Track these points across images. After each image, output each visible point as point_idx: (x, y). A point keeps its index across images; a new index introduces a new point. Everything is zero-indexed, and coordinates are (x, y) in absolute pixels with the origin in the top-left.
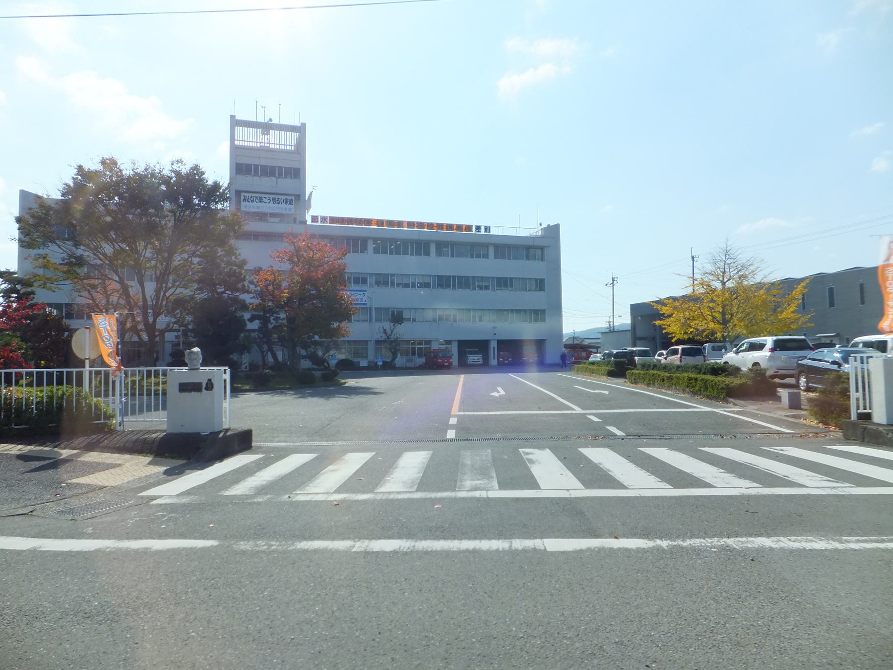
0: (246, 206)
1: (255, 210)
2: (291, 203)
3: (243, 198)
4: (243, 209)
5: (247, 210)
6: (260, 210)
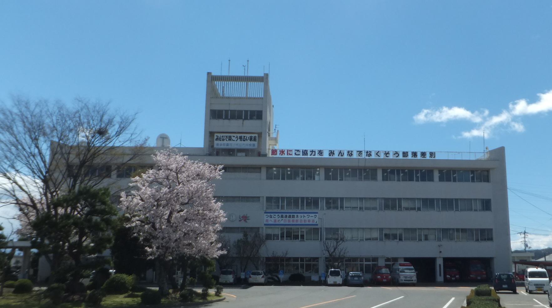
0: (217, 145)
1: (225, 147)
2: (255, 140)
3: (215, 137)
4: (215, 146)
5: (220, 147)
6: (229, 147)
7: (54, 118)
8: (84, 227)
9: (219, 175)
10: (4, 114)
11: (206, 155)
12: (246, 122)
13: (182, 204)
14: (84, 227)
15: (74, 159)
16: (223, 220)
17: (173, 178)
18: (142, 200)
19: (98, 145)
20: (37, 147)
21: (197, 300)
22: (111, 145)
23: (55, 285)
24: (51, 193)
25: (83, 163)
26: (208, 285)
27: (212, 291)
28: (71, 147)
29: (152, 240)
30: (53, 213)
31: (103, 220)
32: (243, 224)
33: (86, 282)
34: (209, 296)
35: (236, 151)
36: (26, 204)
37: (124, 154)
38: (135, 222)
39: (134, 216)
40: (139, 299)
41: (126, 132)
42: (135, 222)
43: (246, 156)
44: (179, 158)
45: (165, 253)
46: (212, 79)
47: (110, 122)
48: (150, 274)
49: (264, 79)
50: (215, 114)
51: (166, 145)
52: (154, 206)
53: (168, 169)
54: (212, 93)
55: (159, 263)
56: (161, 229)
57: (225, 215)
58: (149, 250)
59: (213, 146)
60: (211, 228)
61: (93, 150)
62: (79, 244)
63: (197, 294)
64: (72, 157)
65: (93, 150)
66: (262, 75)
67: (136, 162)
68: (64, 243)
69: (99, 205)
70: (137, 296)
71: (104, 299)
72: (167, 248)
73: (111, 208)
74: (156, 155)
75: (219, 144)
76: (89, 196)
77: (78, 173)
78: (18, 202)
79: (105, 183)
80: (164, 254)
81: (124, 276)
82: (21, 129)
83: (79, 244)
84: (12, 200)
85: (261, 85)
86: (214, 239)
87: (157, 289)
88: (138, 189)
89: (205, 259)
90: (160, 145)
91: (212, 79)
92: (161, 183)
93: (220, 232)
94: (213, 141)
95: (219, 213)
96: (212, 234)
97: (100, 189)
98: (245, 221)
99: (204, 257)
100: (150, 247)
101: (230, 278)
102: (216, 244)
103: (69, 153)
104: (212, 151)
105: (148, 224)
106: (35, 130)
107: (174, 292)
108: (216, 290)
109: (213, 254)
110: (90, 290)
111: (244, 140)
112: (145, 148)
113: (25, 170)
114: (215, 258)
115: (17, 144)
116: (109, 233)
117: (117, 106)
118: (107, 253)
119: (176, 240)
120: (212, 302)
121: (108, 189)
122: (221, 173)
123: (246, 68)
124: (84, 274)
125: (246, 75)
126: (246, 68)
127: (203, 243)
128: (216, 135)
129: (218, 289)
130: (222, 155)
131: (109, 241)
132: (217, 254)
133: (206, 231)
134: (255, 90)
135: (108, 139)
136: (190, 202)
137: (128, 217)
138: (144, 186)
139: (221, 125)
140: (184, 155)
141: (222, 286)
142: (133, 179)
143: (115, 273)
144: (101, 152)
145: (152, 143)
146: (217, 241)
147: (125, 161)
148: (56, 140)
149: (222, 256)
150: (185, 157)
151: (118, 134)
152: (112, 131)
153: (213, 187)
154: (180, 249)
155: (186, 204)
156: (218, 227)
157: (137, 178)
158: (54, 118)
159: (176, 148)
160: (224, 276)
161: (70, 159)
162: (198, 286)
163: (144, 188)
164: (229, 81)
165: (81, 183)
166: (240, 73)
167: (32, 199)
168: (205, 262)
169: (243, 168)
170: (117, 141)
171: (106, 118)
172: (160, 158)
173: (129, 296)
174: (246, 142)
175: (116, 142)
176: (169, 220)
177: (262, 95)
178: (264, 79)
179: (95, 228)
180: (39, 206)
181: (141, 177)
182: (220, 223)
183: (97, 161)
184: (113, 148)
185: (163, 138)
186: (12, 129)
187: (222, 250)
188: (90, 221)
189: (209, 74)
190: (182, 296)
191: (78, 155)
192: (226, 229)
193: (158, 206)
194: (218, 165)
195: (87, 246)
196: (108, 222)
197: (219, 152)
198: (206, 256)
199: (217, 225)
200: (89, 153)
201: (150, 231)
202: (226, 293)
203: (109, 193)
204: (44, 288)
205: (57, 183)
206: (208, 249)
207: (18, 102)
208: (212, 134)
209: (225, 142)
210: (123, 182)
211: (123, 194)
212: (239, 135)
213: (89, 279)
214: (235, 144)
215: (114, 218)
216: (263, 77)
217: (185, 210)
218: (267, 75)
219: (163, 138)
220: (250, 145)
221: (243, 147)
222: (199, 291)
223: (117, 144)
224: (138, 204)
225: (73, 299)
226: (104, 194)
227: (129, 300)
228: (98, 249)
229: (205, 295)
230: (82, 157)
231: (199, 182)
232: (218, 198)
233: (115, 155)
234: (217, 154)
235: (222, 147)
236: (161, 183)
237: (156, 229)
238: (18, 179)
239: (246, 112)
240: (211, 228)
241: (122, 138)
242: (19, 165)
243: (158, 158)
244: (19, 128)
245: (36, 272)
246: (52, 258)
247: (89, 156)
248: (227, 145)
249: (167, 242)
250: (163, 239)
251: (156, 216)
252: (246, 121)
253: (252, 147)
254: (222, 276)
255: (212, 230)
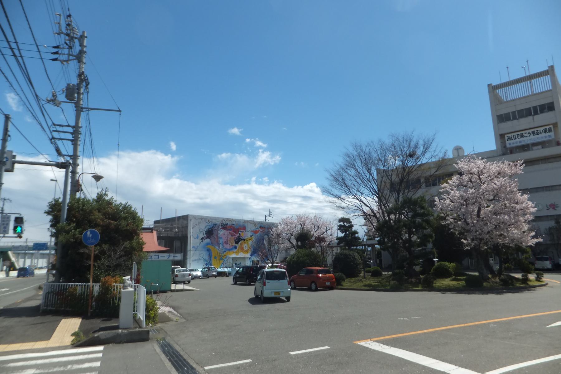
0: (510, 144)
1: (519, 144)
2: (550, 130)
3: (506, 138)
4: (508, 146)
5: (512, 146)
6: (523, 143)
7: (379, 152)
8: (411, 227)
9: (521, 170)
10: (349, 157)
11: (500, 155)
12: (536, 117)
13: (489, 201)
14: (411, 227)
15: (395, 178)
16: (533, 210)
17: (476, 180)
18: (452, 201)
19: (411, 165)
20: (371, 175)
21: (518, 285)
22: (419, 163)
23: (397, 271)
24: (384, 206)
25: (402, 181)
26: (526, 270)
27: (532, 277)
28: (392, 170)
29: (466, 234)
30: (387, 219)
31: (423, 221)
32: (552, 212)
33: (417, 268)
34: (530, 281)
35: (530, 146)
36: (369, 215)
37: (430, 168)
38: (450, 220)
39: (448, 215)
40: (464, 282)
41: (430, 150)
42: (450, 220)
43: (543, 148)
44: (479, 162)
45: (480, 243)
46: (493, 89)
47: (416, 146)
48: (466, 262)
49: (550, 72)
50: (501, 119)
51: (461, 154)
52: (464, 205)
53: (471, 173)
54: (495, 100)
55: (475, 252)
56: (473, 223)
57: (533, 205)
58: (465, 242)
59: (505, 147)
60: (522, 219)
61: (407, 169)
62: (409, 240)
63: (517, 279)
64: (394, 177)
65: (407, 169)
66: (546, 68)
67: (443, 172)
68: (398, 240)
69: (419, 210)
70: (460, 280)
71: (435, 282)
72: (481, 240)
73: (429, 211)
74: (457, 164)
75: (510, 144)
76: (410, 204)
77: (399, 188)
78: (365, 214)
79: (419, 193)
80: (479, 245)
81: (447, 264)
82: (359, 164)
83: (409, 240)
84: (360, 213)
85: (547, 78)
86: (526, 228)
87: (477, 274)
88: (448, 193)
89: (519, 247)
90: (456, 155)
91: (493, 89)
92: (466, 186)
93: (533, 221)
94: (505, 142)
95: (528, 205)
96: (524, 224)
97: (418, 198)
98: (554, 208)
99: (519, 246)
100: (466, 239)
101: (548, 264)
102: (529, 233)
103: (392, 175)
104: (505, 150)
105: (460, 221)
106: (367, 163)
107: (493, 277)
108: (535, 275)
109: (527, 243)
110: (422, 275)
111: (538, 134)
112: (446, 159)
113: (366, 192)
114: (531, 246)
115: (359, 174)
116: (428, 231)
117: (419, 132)
118: (430, 245)
119: (489, 232)
120: (535, 287)
121: (424, 197)
122: (522, 168)
123: (527, 68)
124: (416, 262)
125: (528, 74)
126: (527, 68)
127: (515, 232)
128: (506, 136)
129: (537, 274)
130: (517, 152)
131: (431, 236)
132: (532, 242)
133: (516, 222)
134: (542, 85)
135: (418, 158)
136: (496, 197)
137: (442, 217)
138: (452, 190)
139: (508, 126)
140: (482, 159)
141: (541, 272)
142: (442, 186)
143: (438, 261)
144: (414, 169)
145: (450, 155)
146: (531, 230)
147: (432, 173)
148: (382, 167)
149: (537, 244)
150: (484, 160)
151: (424, 153)
152: (419, 152)
153: (516, 182)
154: (493, 240)
155: (492, 200)
156: (531, 218)
157: (445, 185)
158: (379, 152)
159: (474, 154)
160: (540, 262)
161: (393, 180)
162: (516, 271)
163: (453, 192)
164: (541, 76)
165: (403, 194)
166: (522, 75)
167: (373, 211)
168: (519, 249)
169: (541, 160)
170: (424, 159)
171: (412, 144)
172: (462, 165)
173: (453, 280)
174: (540, 135)
175: (424, 160)
176: (478, 215)
177: (550, 87)
178: (550, 72)
179: (419, 227)
180: (378, 216)
181: (447, 183)
182: (531, 213)
183: (412, 176)
184: (421, 165)
185: (458, 149)
186: (355, 165)
187: (537, 238)
188: (414, 222)
189: (489, 85)
190: (502, 280)
191: (398, 175)
192: (538, 218)
193: (467, 205)
194: (517, 161)
195: (415, 241)
196: (428, 222)
197: (512, 151)
198: (520, 245)
199: (528, 216)
200: (405, 171)
201: (463, 226)
202: (547, 278)
203: (425, 200)
204: (390, 273)
205: (387, 198)
206: (521, 238)
207: (356, 147)
208: (502, 136)
209: (517, 140)
210: (433, 190)
211: (436, 199)
212: (531, 131)
213: (419, 266)
214: (529, 139)
215: (432, 218)
216: (548, 71)
217: (492, 206)
218: (552, 68)
219: (458, 149)
220: (545, 137)
221: (538, 141)
222: (519, 276)
223: (424, 162)
224: (449, 205)
225: (412, 282)
226: (421, 201)
227: (454, 283)
228: (423, 243)
229: (525, 280)
230: (400, 175)
231: (502, 179)
232: (524, 191)
233: (424, 170)
234: (511, 152)
235: (515, 145)
236: (466, 186)
237: (468, 224)
238: (363, 199)
239: (514, 113)
240: (522, 219)
241: (428, 155)
242: (362, 189)
243: (460, 166)
244: (358, 164)
245: (381, 261)
246: (391, 251)
247: (405, 174)
248: (520, 142)
249: (480, 234)
250: (476, 231)
251: (467, 212)
252: (536, 117)
253: (548, 139)
254: (537, 262)
255: (523, 221)
